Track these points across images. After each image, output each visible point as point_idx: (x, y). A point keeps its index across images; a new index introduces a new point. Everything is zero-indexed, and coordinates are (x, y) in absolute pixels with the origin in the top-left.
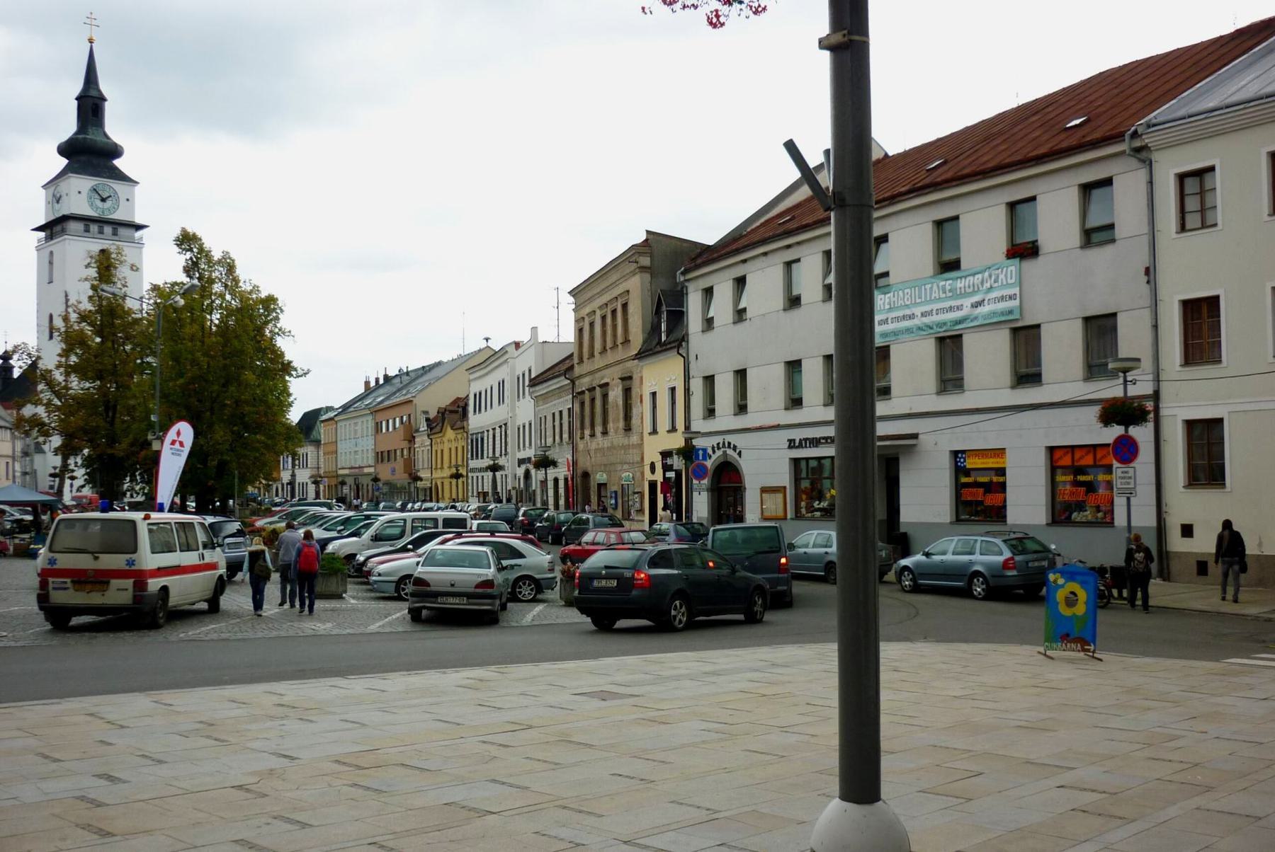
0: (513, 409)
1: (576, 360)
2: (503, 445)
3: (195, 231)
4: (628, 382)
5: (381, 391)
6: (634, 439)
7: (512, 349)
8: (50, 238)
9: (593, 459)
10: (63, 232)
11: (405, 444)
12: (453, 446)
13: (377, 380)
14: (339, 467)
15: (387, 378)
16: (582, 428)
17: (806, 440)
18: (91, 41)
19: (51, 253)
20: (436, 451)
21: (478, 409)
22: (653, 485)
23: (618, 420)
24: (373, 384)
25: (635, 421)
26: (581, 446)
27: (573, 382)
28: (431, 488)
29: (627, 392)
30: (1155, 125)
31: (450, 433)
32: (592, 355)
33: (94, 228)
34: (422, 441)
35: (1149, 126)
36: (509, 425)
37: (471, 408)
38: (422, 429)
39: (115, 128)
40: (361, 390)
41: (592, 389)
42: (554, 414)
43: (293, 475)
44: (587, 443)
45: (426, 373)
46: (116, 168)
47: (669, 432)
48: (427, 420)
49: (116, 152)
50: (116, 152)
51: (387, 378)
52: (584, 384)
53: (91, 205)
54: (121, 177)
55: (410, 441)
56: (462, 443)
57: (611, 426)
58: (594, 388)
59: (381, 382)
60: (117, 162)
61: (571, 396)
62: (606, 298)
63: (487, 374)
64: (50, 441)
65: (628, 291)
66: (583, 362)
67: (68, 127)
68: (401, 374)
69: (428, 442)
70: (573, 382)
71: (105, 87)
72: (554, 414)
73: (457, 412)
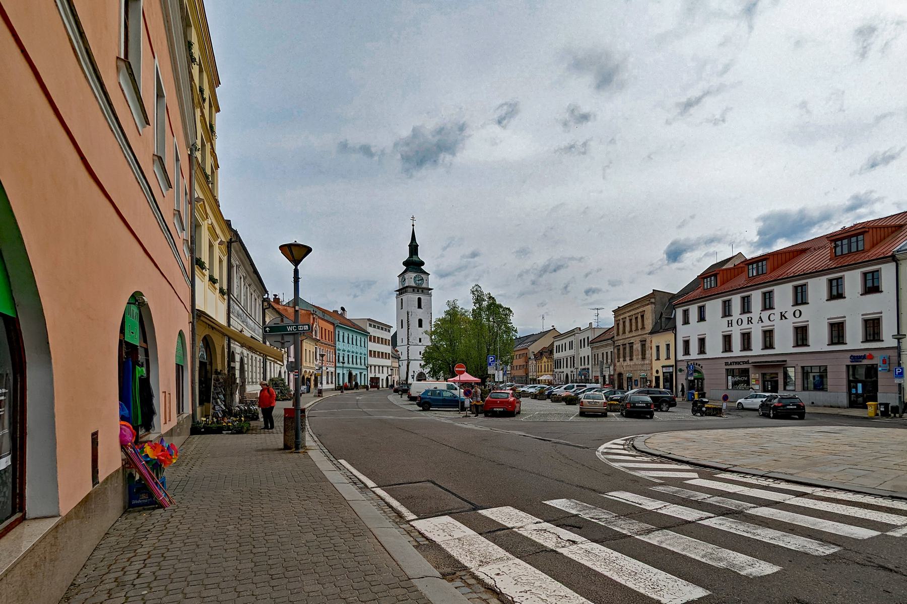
0: (578, 351)
1: (615, 332)
2: (572, 362)
3: (905, 368)
4: (644, 343)
6: (647, 362)
8: (400, 294)
9: (625, 369)
10: (406, 292)
11: (525, 363)
16: (619, 358)
17: (733, 362)
18: (413, 225)
19: (402, 299)
21: (558, 351)
22: (657, 378)
23: (638, 355)
25: (648, 355)
26: (618, 364)
27: (614, 342)
29: (643, 346)
30: (900, 251)
31: (545, 359)
32: (624, 332)
33: (416, 290)
35: (898, 252)
36: (575, 356)
37: (555, 351)
39: (421, 256)
42: (565, 350)
47: (666, 359)
48: (534, 355)
49: (422, 263)
50: (422, 263)
52: (620, 343)
54: (425, 273)
55: (526, 362)
57: (634, 357)
58: (626, 344)
62: (633, 312)
65: (644, 311)
67: (406, 255)
70: (614, 342)
72: (565, 350)
73: (548, 352)
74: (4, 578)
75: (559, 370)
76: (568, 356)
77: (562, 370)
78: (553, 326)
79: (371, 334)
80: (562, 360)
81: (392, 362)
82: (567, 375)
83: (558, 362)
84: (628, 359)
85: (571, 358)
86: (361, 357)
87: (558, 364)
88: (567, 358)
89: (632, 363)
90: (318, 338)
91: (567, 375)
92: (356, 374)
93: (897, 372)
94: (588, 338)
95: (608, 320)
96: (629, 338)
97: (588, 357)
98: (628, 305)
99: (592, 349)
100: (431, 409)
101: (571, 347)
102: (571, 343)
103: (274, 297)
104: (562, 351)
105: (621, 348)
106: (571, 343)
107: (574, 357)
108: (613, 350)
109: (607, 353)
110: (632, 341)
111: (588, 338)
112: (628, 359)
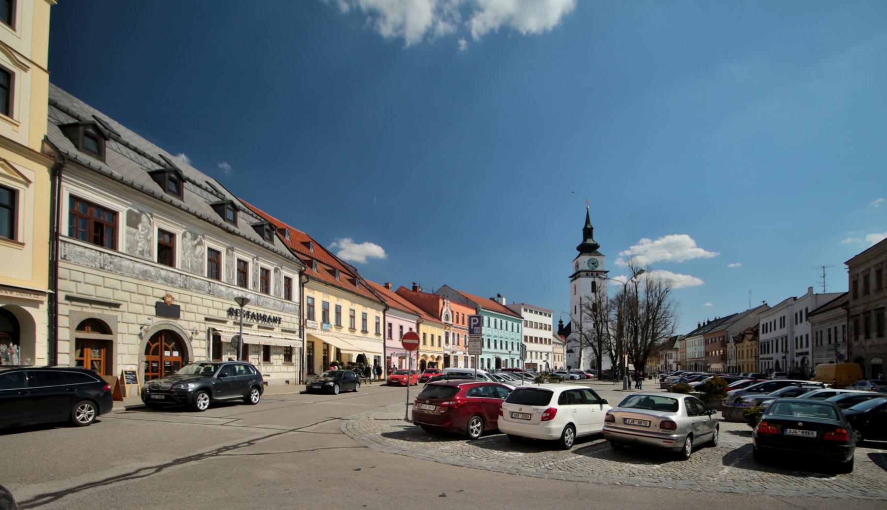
5: (706, 328)
7: (793, 302)
8: (575, 279)
10: (579, 276)
12: (750, 348)
13: (704, 323)
14: (687, 358)
15: (709, 322)
20: (739, 351)
21: (765, 330)
24: (702, 325)
26: (856, 344)
28: (736, 367)
34: (731, 345)
38: (730, 342)
39: (596, 238)
40: (696, 327)
41: (867, 313)
43: (666, 361)
44: (862, 342)
45: (730, 318)
46: (598, 252)
51: (709, 322)
53: (589, 266)
54: (600, 255)
56: (754, 347)
58: (869, 312)
59: (706, 324)
60: (598, 250)
61: (846, 318)
63: (771, 315)
64: (407, 419)
66: (869, 294)
67: (580, 240)
68: (716, 320)
69: (734, 347)
71: (593, 223)
74: (513, 468)
75: (766, 356)
76: (778, 337)
77: (770, 355)
78: (764, 302)
79: (525, 319)
80: (771, 342)
81: (553, 348)
82: (777, 363)
83: (765, 346)
84: (874, 335)
85: (782, 339)
86: (512, 343)
87: (765, 347)
88: (777, 340)
89: (882, 341)
90: (450, 322)
91: (777, 363)
92: (506, 360)
93: (473, 323)
94: (807, 309)
95: (840, 284)
96: (876, 300)
97: (807, 336)
98: (869, 251)
99: (813, 325)
100: (775, 383)
101: (782, 325)
102: (783, 320)
103: (413, 285)
104: (771, 331)
105: (862, 318)
106: (783, 320)
107: (786, 337)
108: (846, 323)
109: (836, 328)
110: (881, 306)
111: (807, 309)
112: (874, 335)
